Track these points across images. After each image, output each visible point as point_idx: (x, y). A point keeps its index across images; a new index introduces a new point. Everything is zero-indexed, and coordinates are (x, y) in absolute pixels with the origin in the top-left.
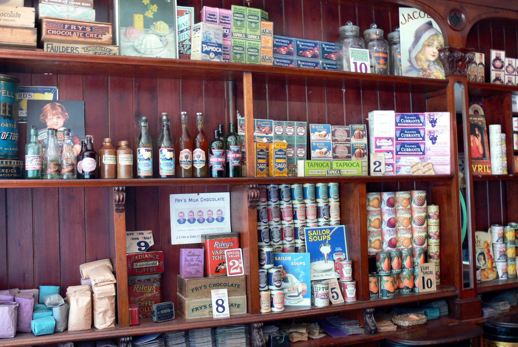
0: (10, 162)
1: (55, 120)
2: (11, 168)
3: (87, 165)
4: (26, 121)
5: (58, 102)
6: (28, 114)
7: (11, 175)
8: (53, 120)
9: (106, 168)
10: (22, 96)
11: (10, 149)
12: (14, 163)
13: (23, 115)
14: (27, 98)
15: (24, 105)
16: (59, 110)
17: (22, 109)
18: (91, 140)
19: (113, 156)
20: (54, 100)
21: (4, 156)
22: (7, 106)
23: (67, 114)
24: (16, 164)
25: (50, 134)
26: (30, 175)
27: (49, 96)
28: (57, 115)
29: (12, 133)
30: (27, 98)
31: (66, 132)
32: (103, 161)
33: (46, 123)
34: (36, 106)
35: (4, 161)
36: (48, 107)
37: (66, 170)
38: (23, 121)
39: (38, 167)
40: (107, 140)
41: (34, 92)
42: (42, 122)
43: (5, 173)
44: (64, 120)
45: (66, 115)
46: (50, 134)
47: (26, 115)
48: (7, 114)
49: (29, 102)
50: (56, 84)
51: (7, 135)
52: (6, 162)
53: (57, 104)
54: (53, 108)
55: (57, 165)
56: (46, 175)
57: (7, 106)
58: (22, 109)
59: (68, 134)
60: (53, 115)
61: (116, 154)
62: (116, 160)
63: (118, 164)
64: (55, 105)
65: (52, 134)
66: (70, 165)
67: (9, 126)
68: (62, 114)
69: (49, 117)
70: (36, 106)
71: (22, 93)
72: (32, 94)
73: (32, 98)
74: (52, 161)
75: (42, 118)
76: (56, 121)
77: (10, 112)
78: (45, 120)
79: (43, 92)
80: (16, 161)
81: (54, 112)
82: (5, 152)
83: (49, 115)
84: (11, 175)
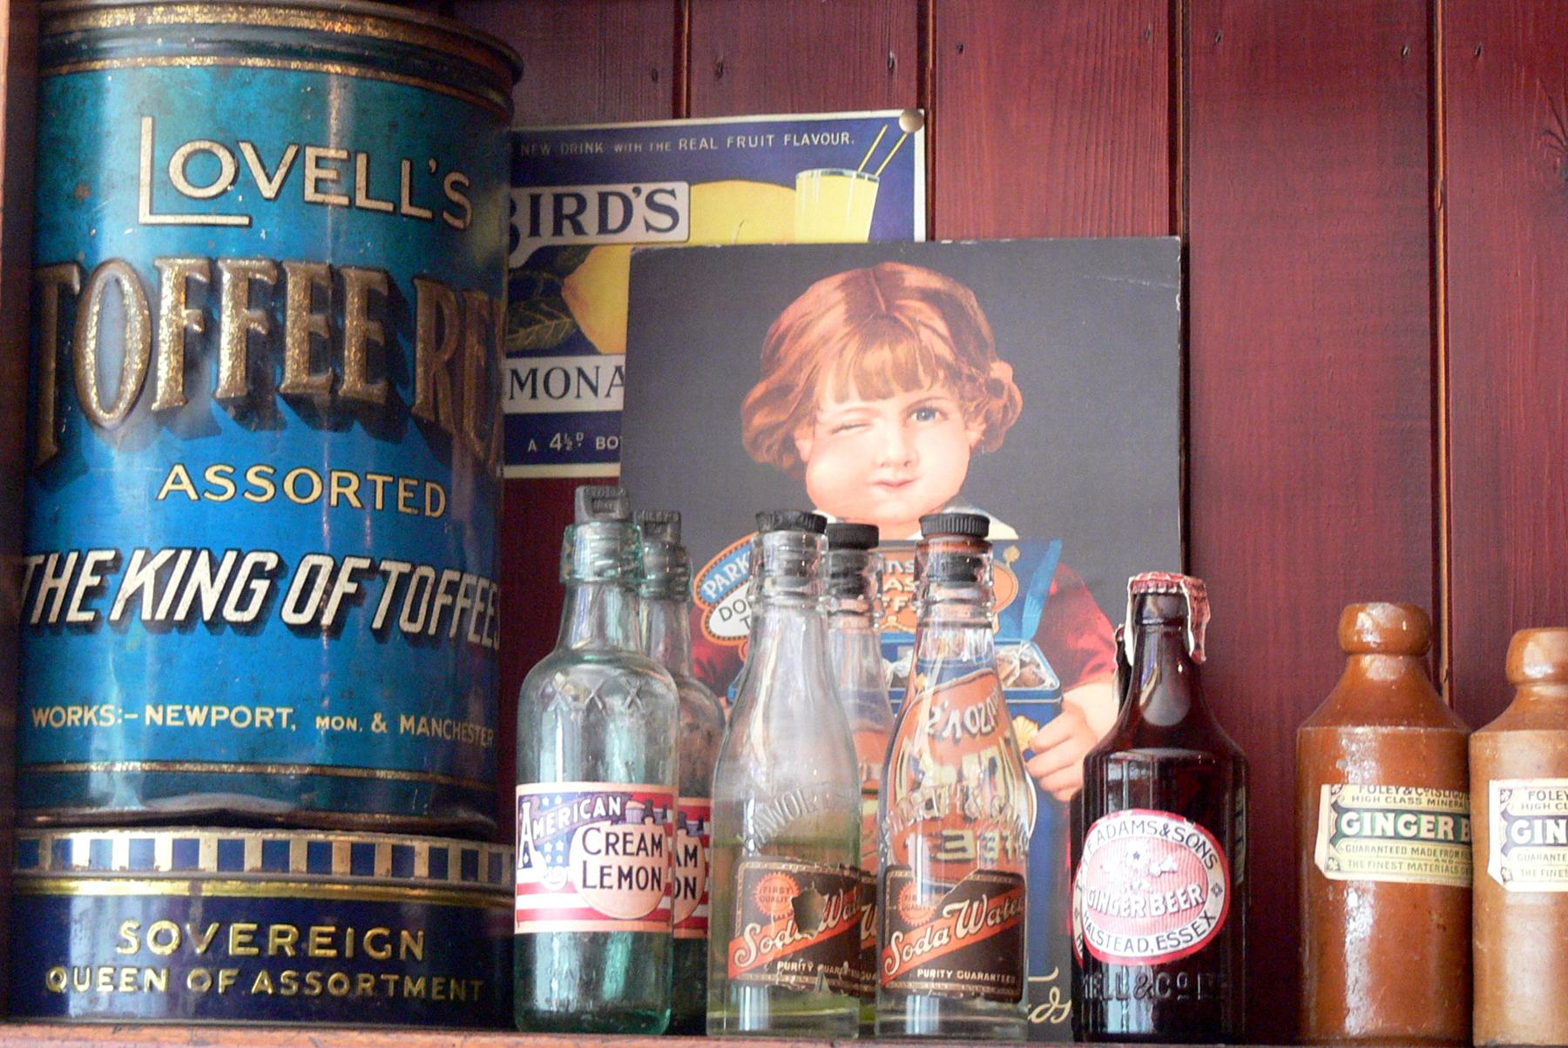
0: (402, 858)
1: (883, 439)
2: (387, 913)
3: (1145, 891)
4: (608, 456)
5: (927, 255)
6: (631, 377)
7: (366, 984)
8: (870, 436)
9: (1360, 923)
10: (590, 219)
11: (378, 724)
12: (420, 865)
13: (588, 403)
14: (636, 233)
15: (603, 299)
16: (933, 332)
17: (577, 344)
18: (1175, 623)
19: (1423, 798)
20: (890, 240)
21: (306, 783)
22: (353, 302)
23: (1001, 371)
24: (421, 869)
25: (776, 566)
26: (554, 985)
27: (833, 207)
28: (911, 383)
29: (394, 568)
30: (636, 233)
31: (939, 549)
32: (1322, 854)
33: (800, 467)
34: (714, 307)
35: (298, 843)
36: (824, 308)
37: (929, 935)
38: (587, 454)
39: (624, 909)
40: (1372, 621)
41: (701, 170)
42: (762, 457)
43: (302, 962)
44: (975, 435)
45: (995, 387)
46: (776, 566)
47: (613, 401)
48: (351, 381)
49: (650, 267)
50: (905, 81)
51: (344, 586)
52: (319, 856)
53: (915, 277)
54: (876, 317)
55: (831, 885)
56: (727, 988)
57: (353, 302)
58: (577, 344)
59: (965, 572)
60: (872, 390)
61: (1460, 776)
62: (1465, 838)
63: (1479, 885)
64: (893, 287)
65: (800, 571)
66: (971, 892)
67: (365, 490)
68: (954, 376)
69: (831, 411)
70: (714, 307)
71: (591, 193)
72: (680, 193)
73: (677, 236)
74: (778, 846)
75: (760, 420)
76: (894, 451)
77: (386, 360)
78: (789, 445)
79: (779, 168)
80: (454, 847)
81: (880, 357)
82: (319, 753)
83: (827, 387)
84: (366, 984)
